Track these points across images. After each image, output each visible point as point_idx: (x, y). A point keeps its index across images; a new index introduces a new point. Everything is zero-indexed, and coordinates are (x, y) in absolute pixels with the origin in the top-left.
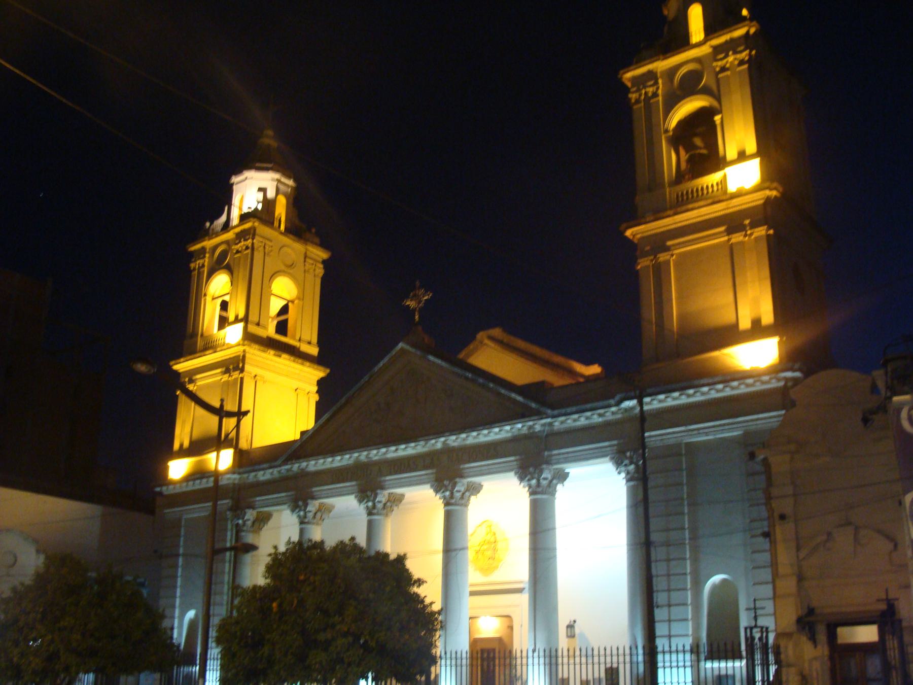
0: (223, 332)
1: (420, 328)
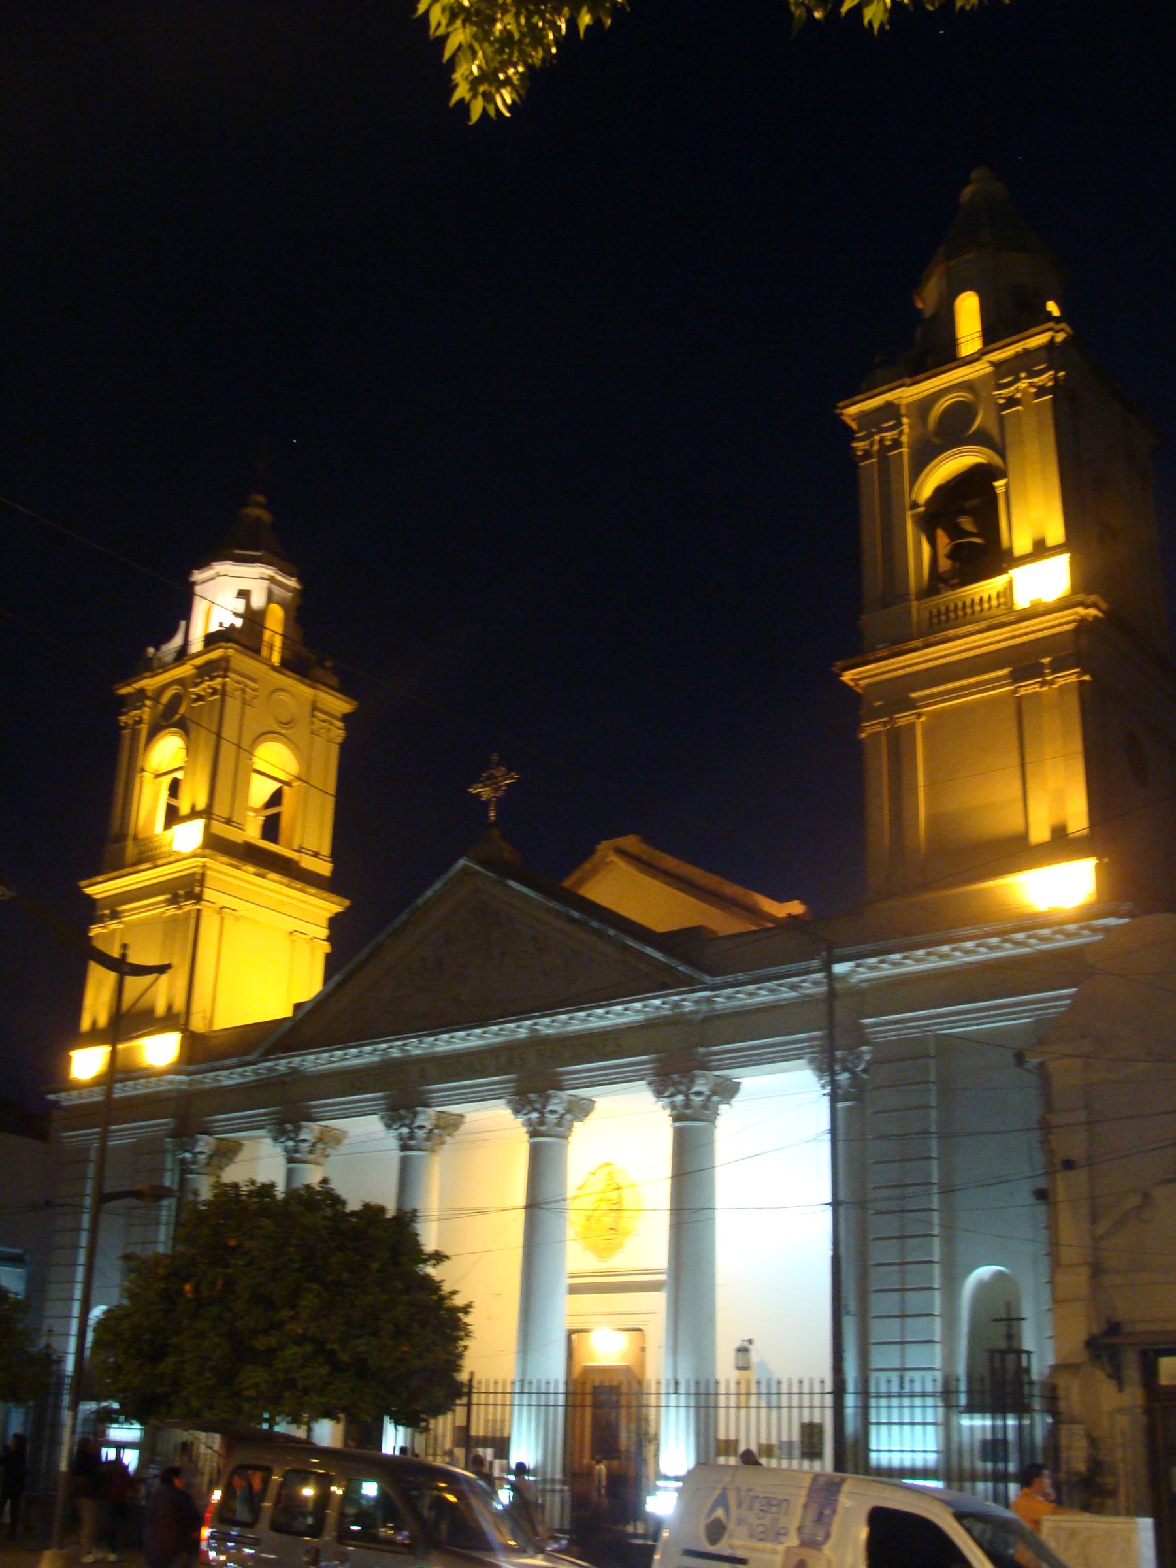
0: (169, 832)
1: (496, 833)
